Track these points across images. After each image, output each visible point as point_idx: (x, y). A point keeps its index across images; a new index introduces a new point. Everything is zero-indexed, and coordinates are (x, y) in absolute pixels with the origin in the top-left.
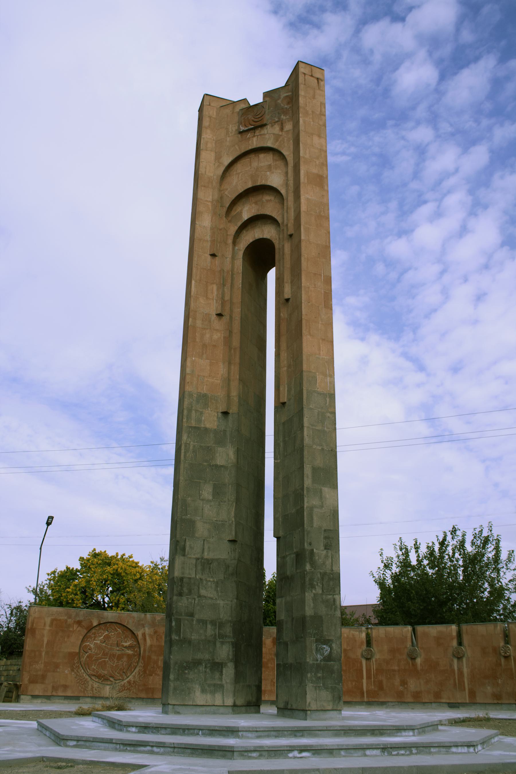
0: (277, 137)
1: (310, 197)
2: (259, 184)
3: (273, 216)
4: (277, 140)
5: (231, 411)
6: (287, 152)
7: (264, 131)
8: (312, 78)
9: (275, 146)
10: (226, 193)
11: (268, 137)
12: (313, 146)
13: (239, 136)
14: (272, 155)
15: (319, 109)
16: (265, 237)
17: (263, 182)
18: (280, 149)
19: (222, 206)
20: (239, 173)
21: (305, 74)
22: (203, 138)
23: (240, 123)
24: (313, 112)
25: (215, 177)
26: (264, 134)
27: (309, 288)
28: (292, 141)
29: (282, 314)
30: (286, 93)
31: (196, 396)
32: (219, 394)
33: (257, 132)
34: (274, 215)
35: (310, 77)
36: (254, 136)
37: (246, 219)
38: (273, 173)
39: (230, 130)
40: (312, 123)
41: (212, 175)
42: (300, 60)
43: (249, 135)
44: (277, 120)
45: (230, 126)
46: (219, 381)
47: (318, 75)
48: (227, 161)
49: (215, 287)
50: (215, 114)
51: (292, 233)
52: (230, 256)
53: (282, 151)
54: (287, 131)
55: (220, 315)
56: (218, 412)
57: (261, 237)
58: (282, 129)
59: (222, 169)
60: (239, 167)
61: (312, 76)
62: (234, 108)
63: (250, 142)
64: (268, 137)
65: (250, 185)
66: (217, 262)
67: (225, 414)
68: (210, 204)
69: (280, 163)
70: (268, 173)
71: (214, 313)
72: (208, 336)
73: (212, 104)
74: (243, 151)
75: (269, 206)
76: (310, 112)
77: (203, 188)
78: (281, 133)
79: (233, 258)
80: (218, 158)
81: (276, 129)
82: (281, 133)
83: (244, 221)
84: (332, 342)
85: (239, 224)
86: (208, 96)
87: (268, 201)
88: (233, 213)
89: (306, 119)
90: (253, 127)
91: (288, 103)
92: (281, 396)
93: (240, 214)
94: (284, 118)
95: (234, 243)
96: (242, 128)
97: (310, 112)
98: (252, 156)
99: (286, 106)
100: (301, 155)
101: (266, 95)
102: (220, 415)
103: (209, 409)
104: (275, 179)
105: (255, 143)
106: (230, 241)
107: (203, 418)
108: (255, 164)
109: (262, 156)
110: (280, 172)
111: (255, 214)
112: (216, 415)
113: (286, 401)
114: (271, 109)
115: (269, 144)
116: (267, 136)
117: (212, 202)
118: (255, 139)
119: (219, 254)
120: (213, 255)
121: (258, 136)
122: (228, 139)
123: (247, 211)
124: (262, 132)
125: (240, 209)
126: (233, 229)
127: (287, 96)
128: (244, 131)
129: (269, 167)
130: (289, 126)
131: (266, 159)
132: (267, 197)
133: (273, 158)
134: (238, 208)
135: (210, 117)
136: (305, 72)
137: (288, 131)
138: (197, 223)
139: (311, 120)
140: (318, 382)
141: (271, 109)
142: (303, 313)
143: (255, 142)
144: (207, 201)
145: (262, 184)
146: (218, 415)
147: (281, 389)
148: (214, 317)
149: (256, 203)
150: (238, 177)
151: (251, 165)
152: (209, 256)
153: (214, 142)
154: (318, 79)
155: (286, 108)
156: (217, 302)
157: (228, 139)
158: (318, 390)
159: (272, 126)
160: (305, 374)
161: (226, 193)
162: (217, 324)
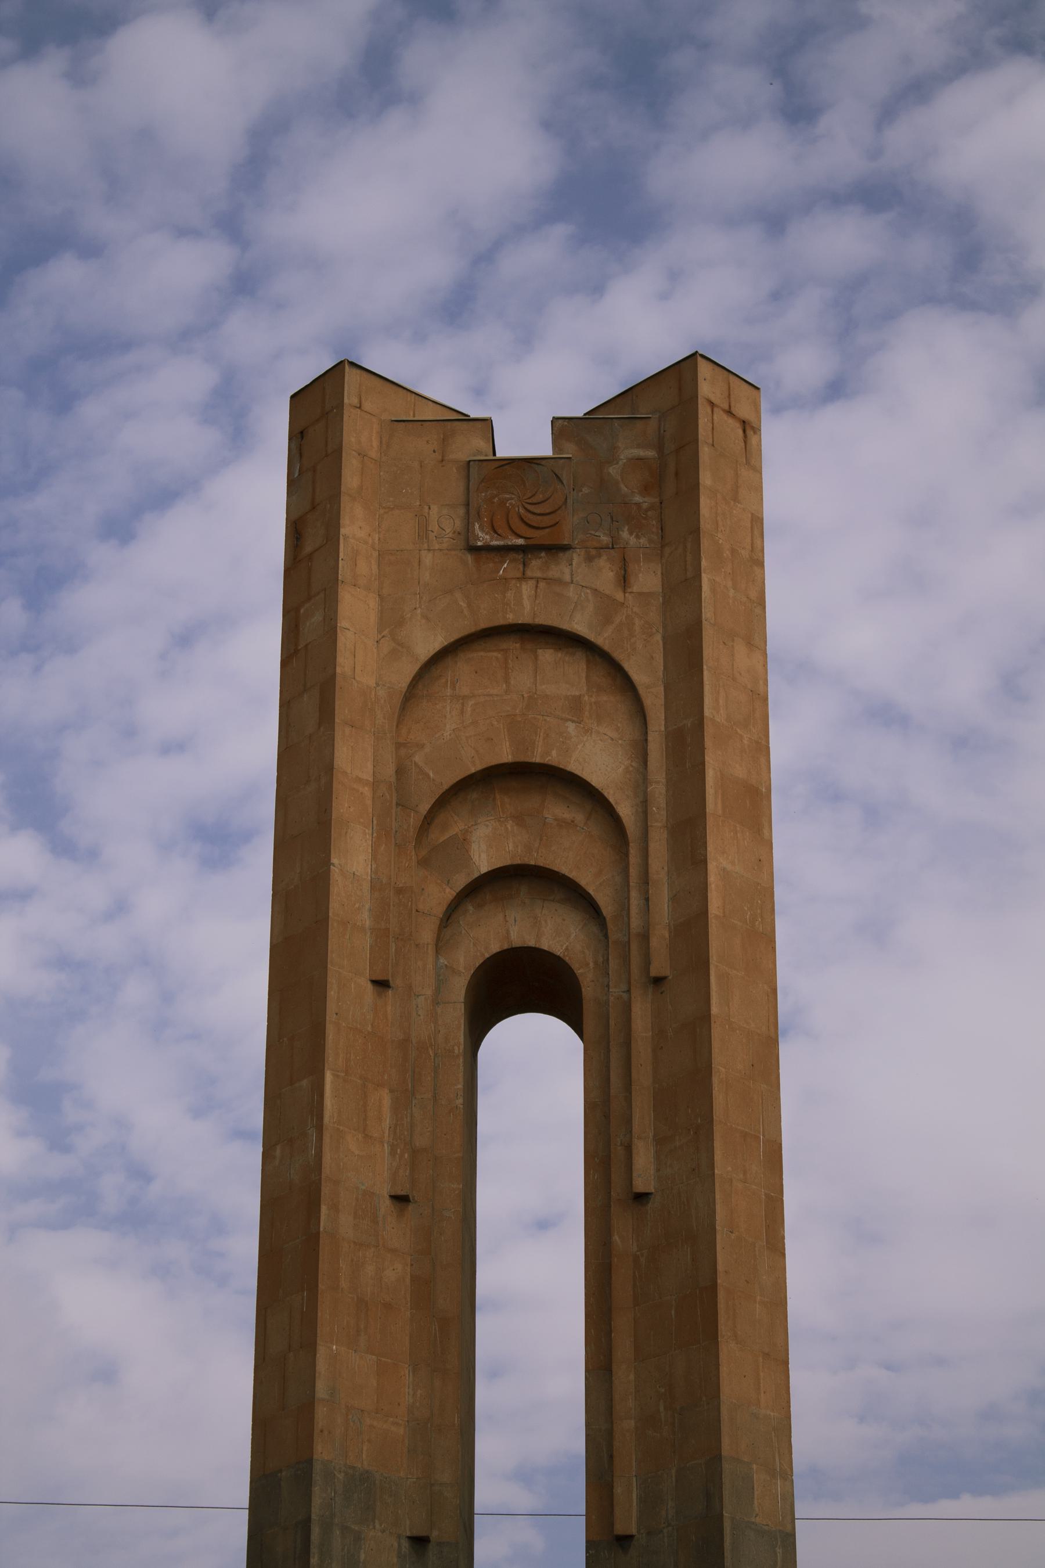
0: (607, 608)
1: (729, 867)
2: (538, 760)
3: (583, 883)
4: (607, 620)
5: (434, 1535)
6: (646, 670)
7: (561, 569)
8: (730, 421)
9: (602, 639)
10: (417, 758)
11: (576, 593)
12: (734, 679)
13: (469, 558)
14: (583, 665)
15: (749, 540)
16: (545, 947)
17: (553, 758)
18: (618, 655)
19: (402, 804)
20: (464, 697)
21: (712, 404)
22: (346, 537)
23: (470, 512)
24: (733, 551)
25: (382, 693)
26: (559, 582)
27: (731, 1180)
28: (658, 638)
29: (616, 1238)
30: (639, 446)
31: (341, 1476)
32: (402, 1474)
33: (536, 565)
34: (586, 880)
35: (725, 417)
36: (524, 578)
37: (484, 870)
38: (588, 731)
39: (434, 526)
40: (732, 593)
41: (372, 683)
42: (700, 352)
43: (506, 567)
44: (605, 539)
45: (435, 508)
46: (401, 1431)
47: (743, 411)
48: (427, 642)
49: (387, 1100)
50: (375, 443)
51: (662, 974)
52: (429, 992)
53: (626, 666)
54: (640, 594)
55: (401, 1200)
56: (399, 1537)
57: (532, 943)
58: (624, 581)
59: (408, 670)
60: (462, 670)
61: (729, 412)
62: (445, 441)
63: (510, 595)
64: (576, 593)
65: (505, 755)
66: (389, 1008)
67: (420, 1542)
68: (367, 791)
69: (612, 701)
70: (571, 727)
71: (384, 1191)
72: (370, 1269)
73: (367, 406)
74: (483, 625)
75: (573, 849)
76: (727, 553)
77: (347, 730)
78: (619, 596)
79: (437, 1000)
80: (391, 621)
81: (605, 575)
82: (619, 596)
83: (476, 875)
84: (786, 1363)
85: (461, 881)
86: (355, 371)
87: (562, 824)
88: (437, 836)
89: (717, 579)
90: (520, 542)
91: (646, 490)
92: (618, 1512)
93: (462, 843)
94: (633, 540)
95: (440, 944)
96: (483, 537)
97: (727, 553)
98: (513, 645)
99: (638, 499)
100: (707, 712)
101: (563, 428)
102: (405, 1544)
103: (377, 1526)
104: (598, 756)
105: (527, 603)
106: (427, 935)
107: (362, 1556)
108: (522, 679)
109: (547, 655)
110: (615, 735)
111: (518, 861)
112: (396, 1545)
113: (634, 1532)
114: (585, 490)
115: (580, 625)
116: (571, 592)
117: (375, 785)
118: (527, 589)
119: (397, 982)
120: (381, 984)
121: (538, 580)
122: (428, 559)
123: (489, 842)
124: (554, 572)
125: (461, 826)
126: (437, 896)
127: (640, 459)
128: (488, 549)
129: (576, 706)
130: (648, 579)
131: (561, 676)
132: (558, 809)
133: (587, 677)
134: (455, 823)
135: (362, 455)
136: (713, 399)
137: (644, 597)
138: (335, 860)
139: (730, 584)
140: (756, 1493)
141: (585, 490)
142: (720, 1267)
143: (526, 604)
144: (359, 780)
145: (547, 760)
146: (399, 1546)
147: (618, 1490)
148: (385, 1205)
149: (519, 819)
150: (462, 712)
151: (507, 679)
152: (370, 986)
153: (375, 554)
154: (744, 423)
155: (638, 505)
156: (393, 1153)
157: (428, 559)
158: (758, 1520)
159: (589, 559)
160: (726, 1466)
161: (417, 758)
162: (396, 1231)
